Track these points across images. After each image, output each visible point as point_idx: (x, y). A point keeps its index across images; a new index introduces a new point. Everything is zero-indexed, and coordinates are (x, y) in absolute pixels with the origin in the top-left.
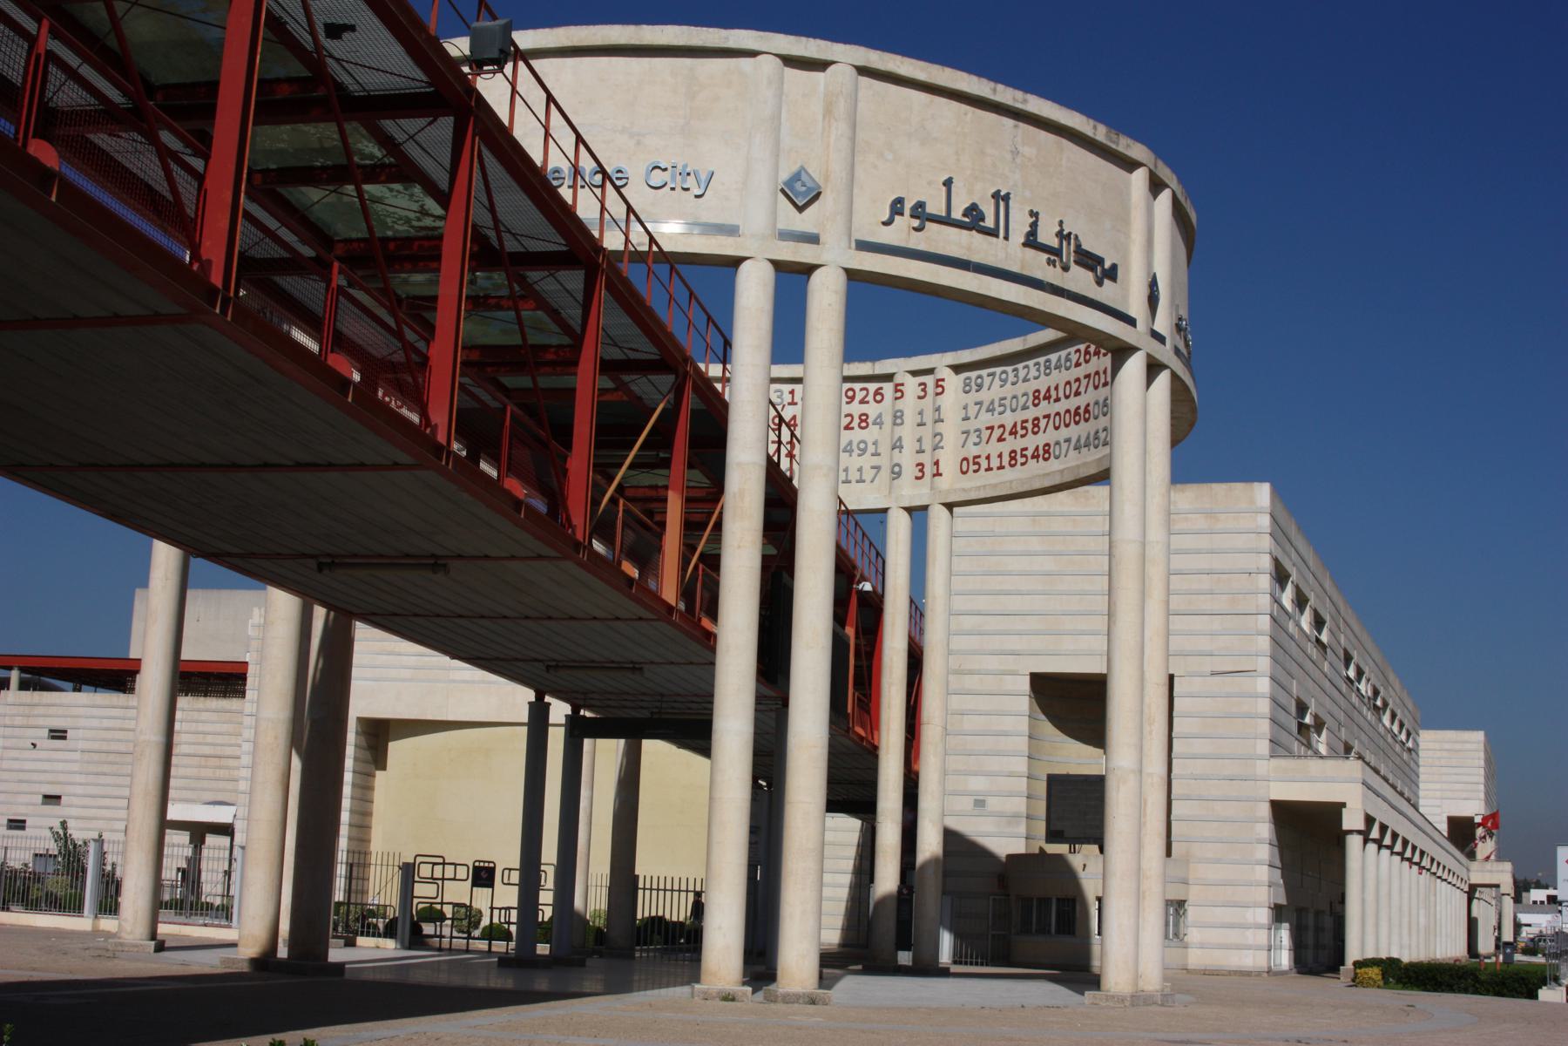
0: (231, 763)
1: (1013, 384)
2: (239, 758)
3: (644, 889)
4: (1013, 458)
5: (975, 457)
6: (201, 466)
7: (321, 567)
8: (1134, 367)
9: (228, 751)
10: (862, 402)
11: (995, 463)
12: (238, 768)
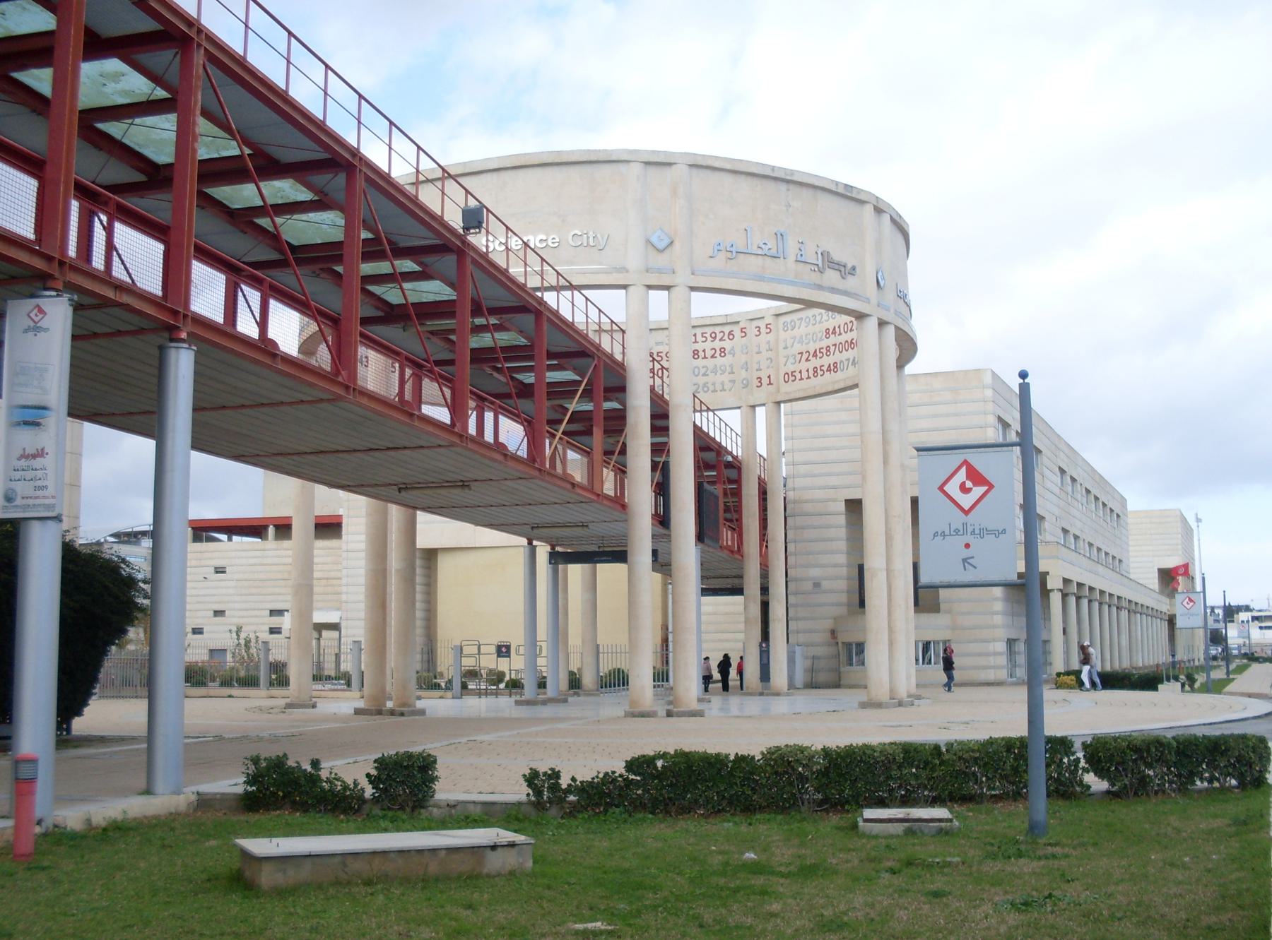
0: (334, 582)
1: (813, 325)
2: (340, 579)
3: (603, 653)
4: (815, 372)
5: (792, 372)
6: (338, 451)
7: (400, 490)
8: (872, 324)
9: (333, 574)
10: (721, 340)
11: (805, 375)
12: (340, 585)
